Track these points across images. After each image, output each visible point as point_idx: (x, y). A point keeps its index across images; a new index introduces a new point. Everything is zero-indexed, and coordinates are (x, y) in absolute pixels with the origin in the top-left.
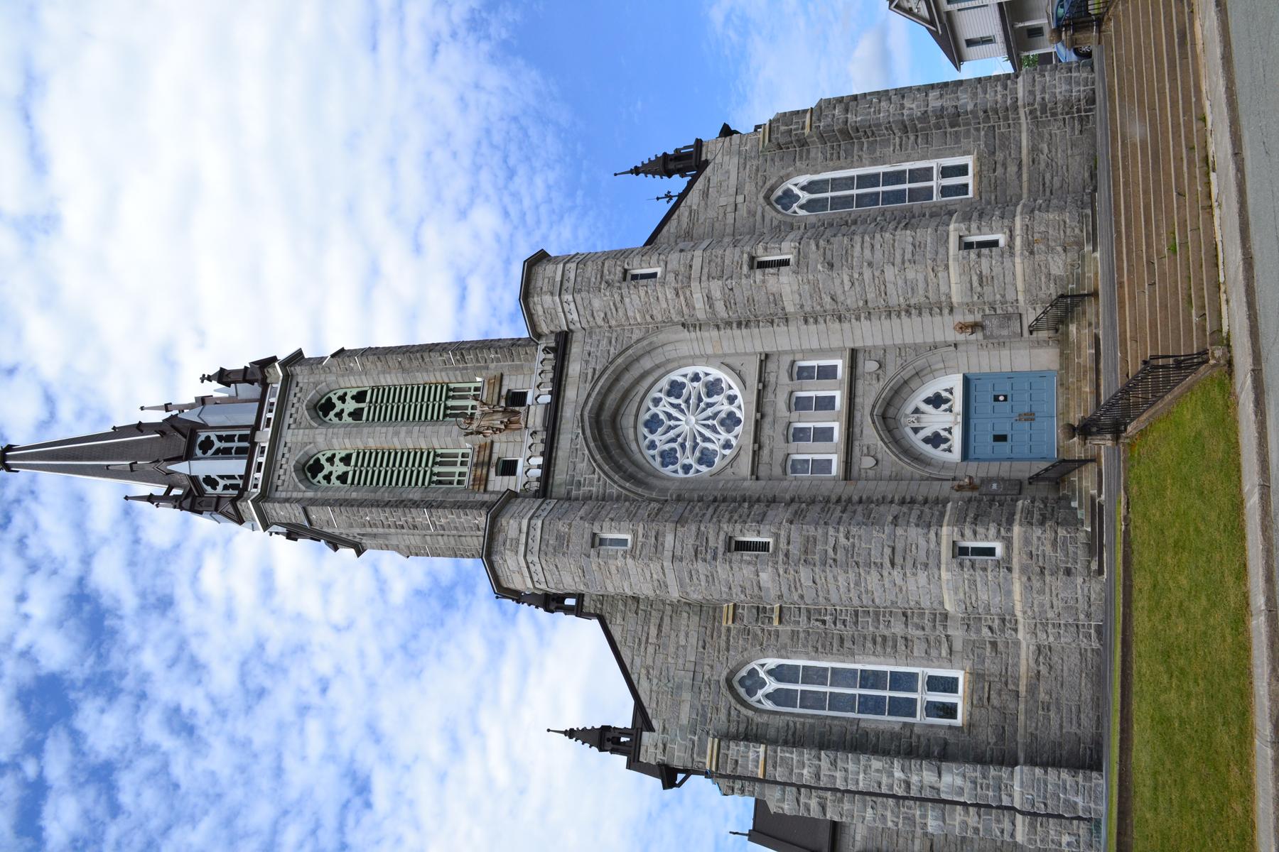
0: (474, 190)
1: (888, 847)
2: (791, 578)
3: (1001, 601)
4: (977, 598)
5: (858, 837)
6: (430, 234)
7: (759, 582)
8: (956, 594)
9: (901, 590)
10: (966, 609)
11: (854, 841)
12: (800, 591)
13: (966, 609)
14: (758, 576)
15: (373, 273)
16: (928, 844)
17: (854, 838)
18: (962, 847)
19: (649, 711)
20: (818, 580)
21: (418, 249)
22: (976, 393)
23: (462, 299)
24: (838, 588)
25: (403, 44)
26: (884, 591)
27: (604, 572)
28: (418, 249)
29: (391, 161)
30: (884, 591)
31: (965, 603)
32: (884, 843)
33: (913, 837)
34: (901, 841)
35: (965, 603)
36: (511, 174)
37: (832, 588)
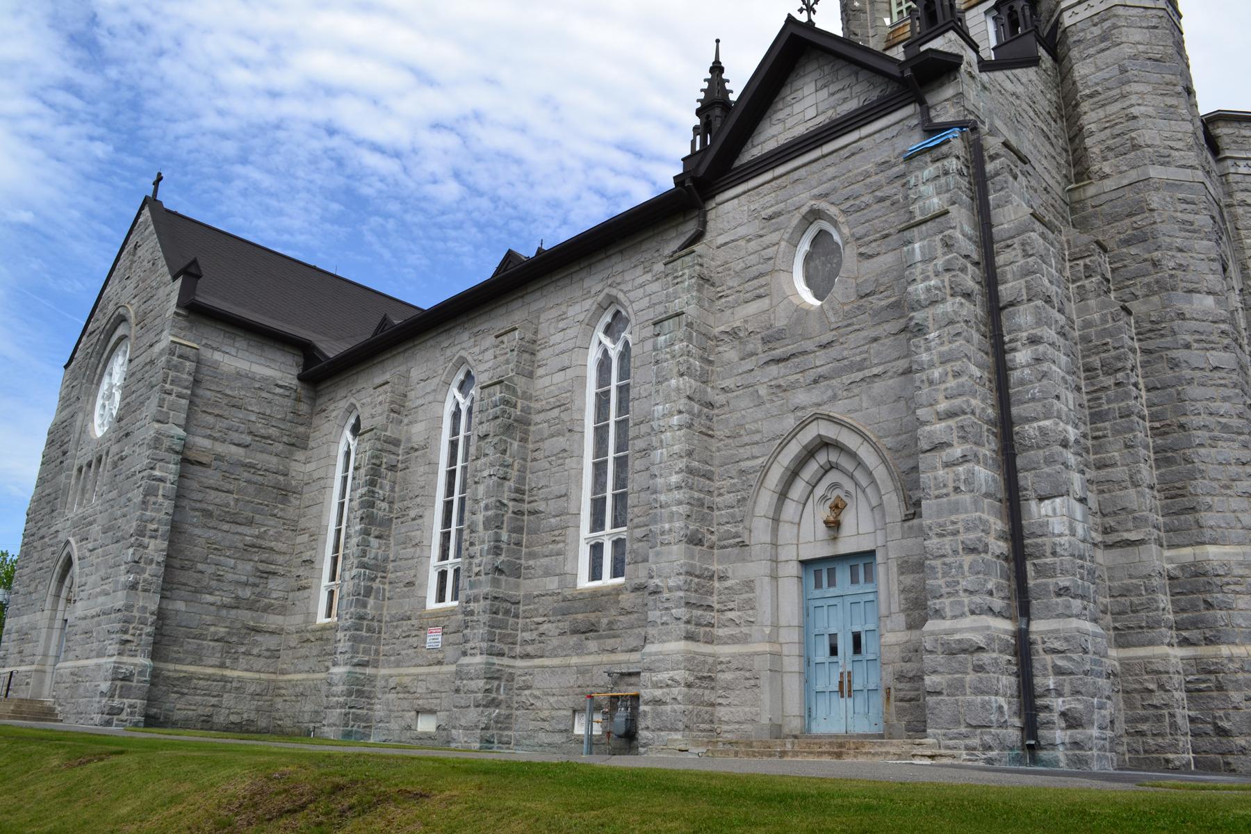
0: (476, 192)
1: (201, 397)
2: (1214, 338)
3: (1239, 626)
4: (1237, 593)
5: (217, 356)
6: (448, 141)
7: (1199, 292)
8: (1240, 564)
9: (1227, 487)
10: (1218, 575)
11: (212, 348)
12: (1195, 345)
13: (1218, 575)
14: (1209, 293)
15: (423, 77)
16: (204, 460)
17: (217, 349)
18: (196, 510)
19: (1018, 72)
20: (1217, 374)
21: (437, 126)
22: (825, 608)
23: (376, 148)
24: (1212, 399)
25: (616, 172)
26: (1220, 464)
27: (1162, 87)
28: (437, 126)
29: (522, 129)
30: (1220, 464)
31: (1227, 575)
32: (208, 393)
33: (215, 439)
34: (211, 419)
35: (1227, 575)
36: (481, 227)
37: (1210, 392)
